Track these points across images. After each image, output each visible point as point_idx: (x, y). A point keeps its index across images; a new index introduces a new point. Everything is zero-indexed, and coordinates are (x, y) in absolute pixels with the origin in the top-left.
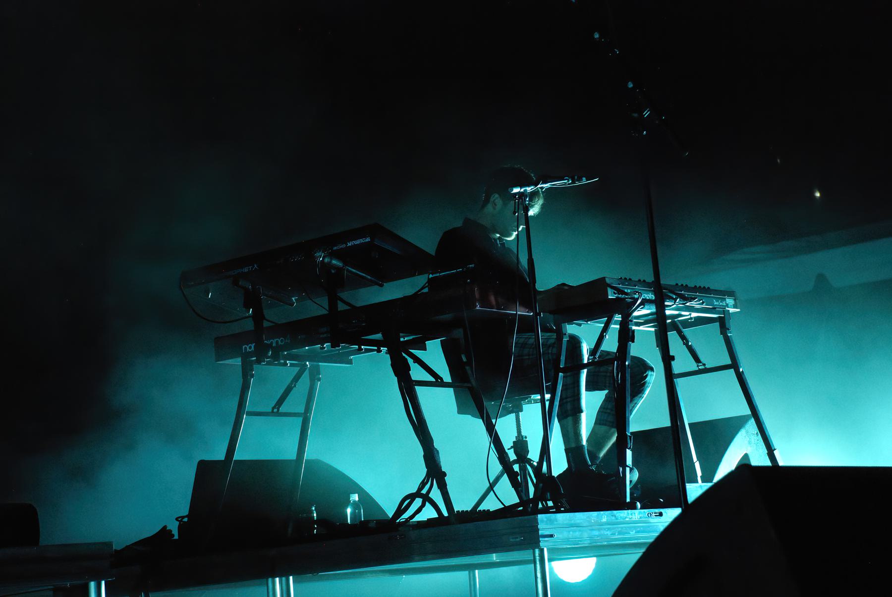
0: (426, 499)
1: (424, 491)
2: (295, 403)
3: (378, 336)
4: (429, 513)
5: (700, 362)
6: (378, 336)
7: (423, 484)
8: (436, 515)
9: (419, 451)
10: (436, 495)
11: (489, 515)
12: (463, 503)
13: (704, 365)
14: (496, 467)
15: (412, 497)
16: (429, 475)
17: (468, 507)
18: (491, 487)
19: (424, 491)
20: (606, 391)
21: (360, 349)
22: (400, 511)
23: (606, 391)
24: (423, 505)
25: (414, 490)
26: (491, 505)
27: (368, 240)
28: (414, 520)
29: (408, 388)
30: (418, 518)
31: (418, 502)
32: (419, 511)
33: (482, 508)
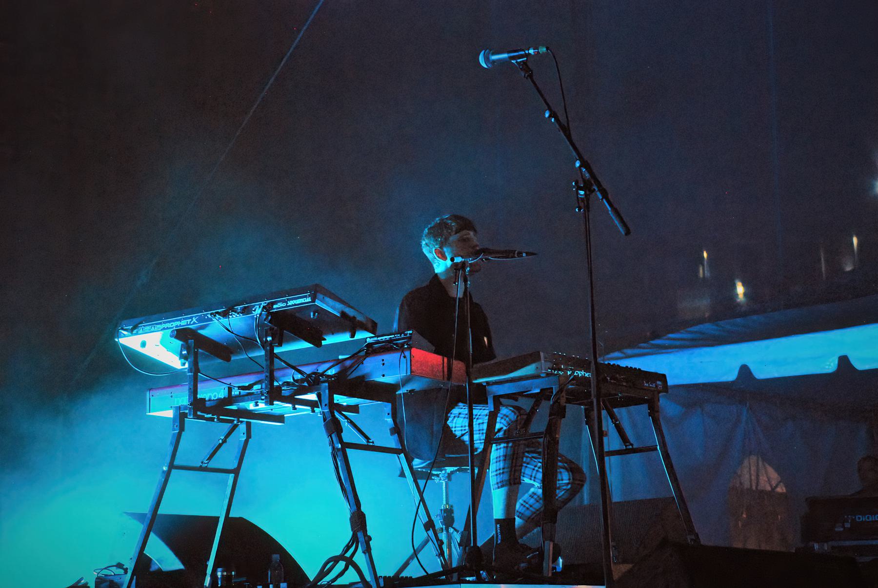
0: (350, 562)
1: (348, 555)
2: (227, 458)
3: (312, 397)
4: (351, 576)
5: (629, 442)
6: (312, 397)
7: (348, 547)
8: (357, 579)
9: (345, 511)
10: (360, 558)
11: (410, 581)
12: (386, 570)
13: (632, 445)
14: (421, 534)
15: (335, 560)
16: (355, 539)
17: (391, 573)
18: (415, 553)
19: (348, 555)
20: (181, 567)
21: (294, 408)
22: (322, 574)
23: (181, 567)
24: (346, 568)
25: (338, 552)
26: (413, 571)
27: (309, 300)
28: (335, 583)
29: (341, 454)
30: (339, 582)
31: (341, 565)
32: (370, 338)
33: (404, 574)
